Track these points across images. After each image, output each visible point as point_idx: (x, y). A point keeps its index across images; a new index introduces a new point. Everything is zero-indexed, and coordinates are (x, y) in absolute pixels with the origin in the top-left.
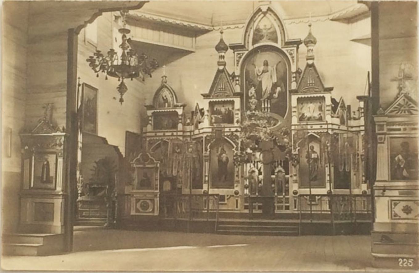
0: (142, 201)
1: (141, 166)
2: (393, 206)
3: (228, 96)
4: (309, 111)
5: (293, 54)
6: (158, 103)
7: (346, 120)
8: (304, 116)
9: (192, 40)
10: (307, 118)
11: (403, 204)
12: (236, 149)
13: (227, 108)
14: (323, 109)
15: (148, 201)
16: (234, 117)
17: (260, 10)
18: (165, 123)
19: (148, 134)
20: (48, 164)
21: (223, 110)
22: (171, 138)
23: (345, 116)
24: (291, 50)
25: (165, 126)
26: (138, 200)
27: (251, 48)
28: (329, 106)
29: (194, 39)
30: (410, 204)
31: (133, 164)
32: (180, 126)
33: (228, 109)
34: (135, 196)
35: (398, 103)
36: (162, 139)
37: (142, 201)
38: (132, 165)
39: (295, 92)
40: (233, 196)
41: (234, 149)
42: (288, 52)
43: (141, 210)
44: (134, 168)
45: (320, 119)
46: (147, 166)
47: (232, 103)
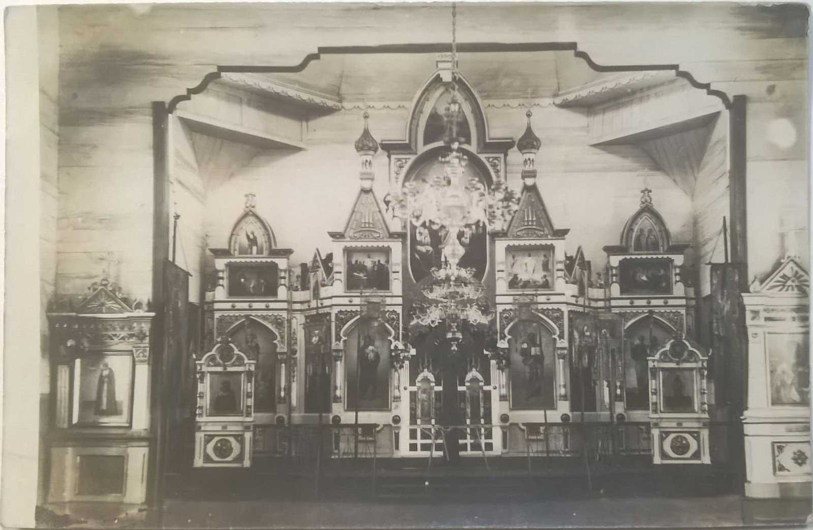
0: (216, 439)
1: (220, 369)
2: (777, 453)
3: (377, 239)
4: (526, 271)
5: (498, 165)
6: (237, 248)
7: (586, 287)
8: (517, 278)
9: (302, 125)
10: (521, 284)
11: (796, 448)
12: (394, 338)
13: (376, 259)
14: (550, 267)
15: (232, 439)
16: (391, 278)
17: (438, 79)
18: (252, 286)
19: (217, 306)
20: (111, 378)
21: (368, 263)
22: (264, 313)
23: (585, 280)
24: (496, 158)
25: (252, 290)
26: (209, 438)
27: (422, 149)
28: (560, 262)
29: (304, 124)
30: (804, 448)
31: (201, 365)
32: (282, 292)
33: (379, 261)
34: (203, 429)
35: (781, 274)
36: (247, 317)
37: (216, 439)
38: (199, 368)
39: (503, 234)
40: (390, 425)
41: (391, 338)
42: (489, 162)
43: (216, 458)
44: (204, 372)
45: (546, 285)
46: (230, 369)
47: (387, 251)
